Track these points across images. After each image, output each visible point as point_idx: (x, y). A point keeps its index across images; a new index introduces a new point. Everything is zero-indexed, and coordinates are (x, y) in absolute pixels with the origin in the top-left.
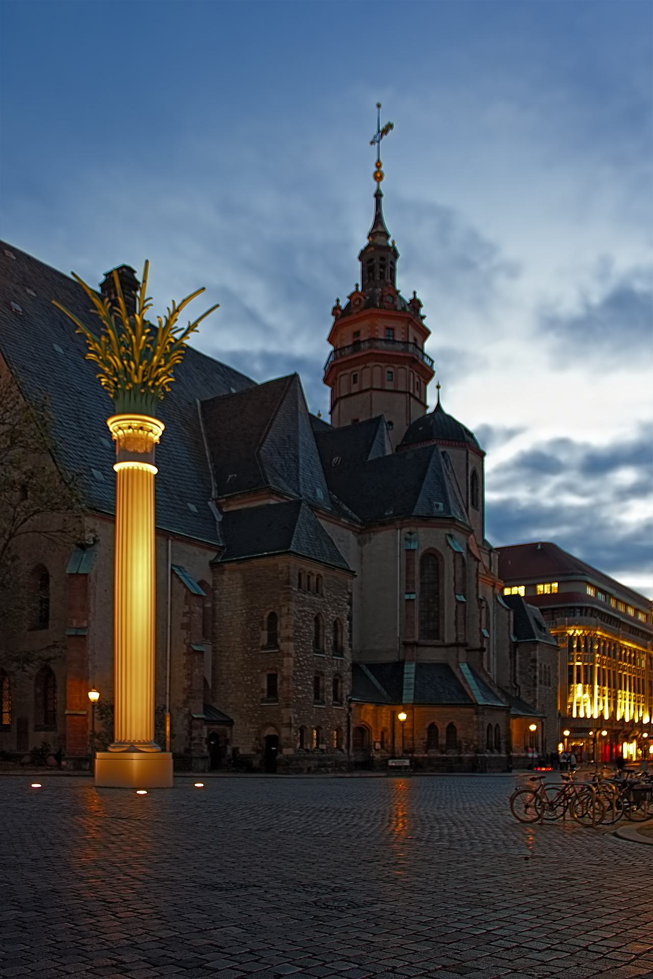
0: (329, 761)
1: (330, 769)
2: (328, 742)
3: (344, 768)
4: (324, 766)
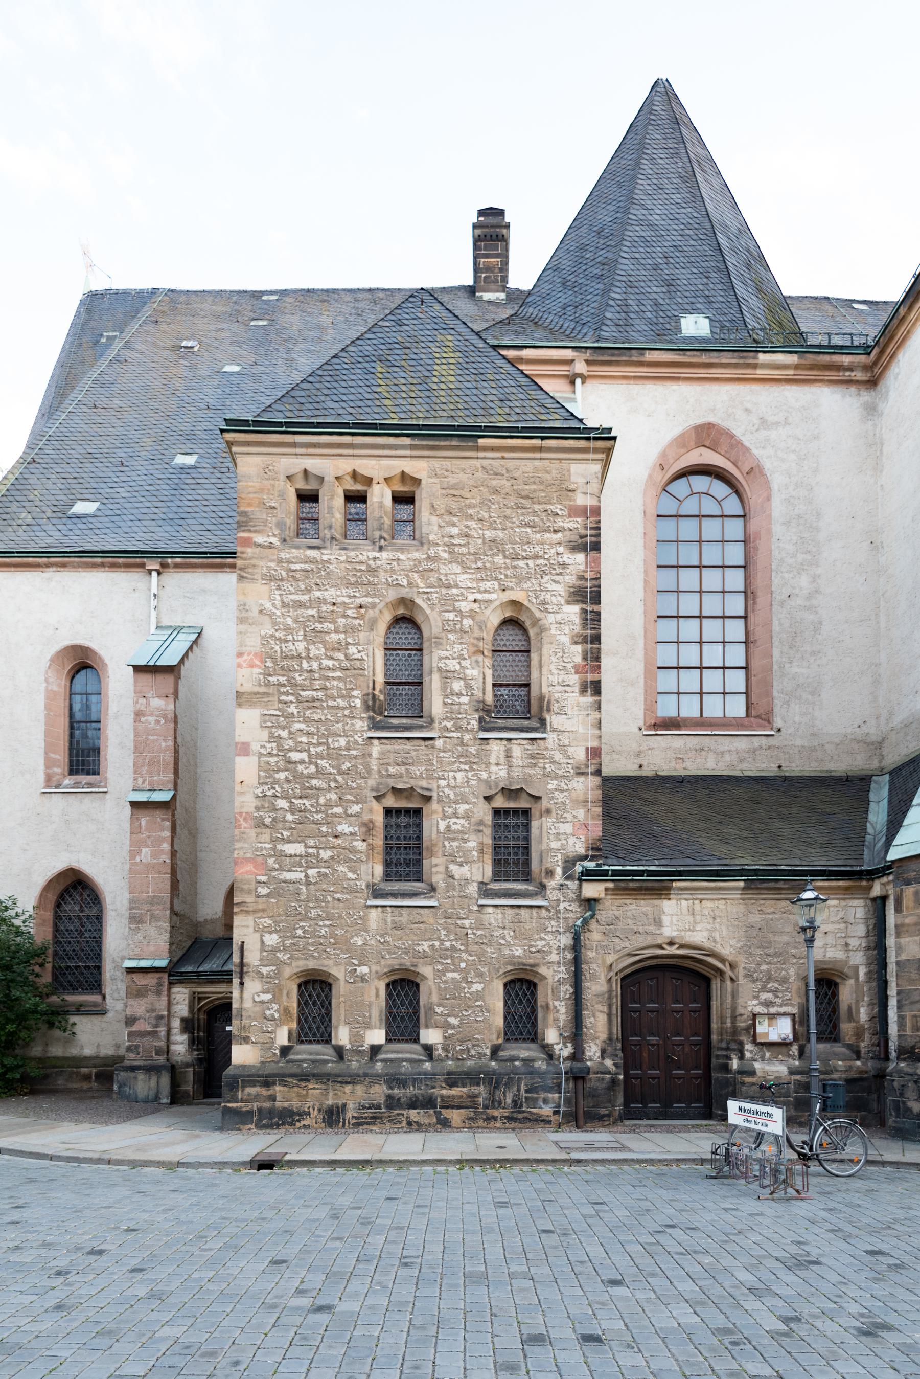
0: (452, 1085)
1: (455, 1116)
2: (453, 1021)
3: (546, 1110)
4: (428, 1103)
